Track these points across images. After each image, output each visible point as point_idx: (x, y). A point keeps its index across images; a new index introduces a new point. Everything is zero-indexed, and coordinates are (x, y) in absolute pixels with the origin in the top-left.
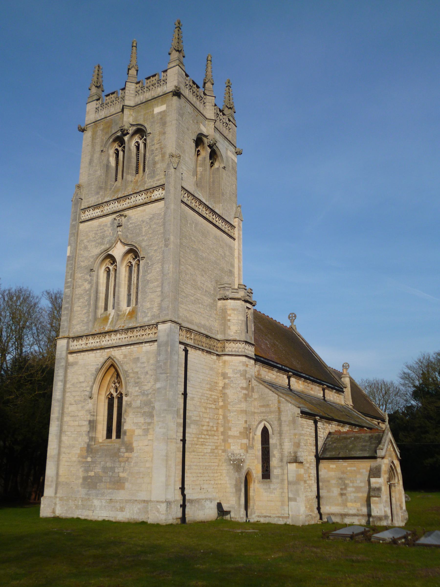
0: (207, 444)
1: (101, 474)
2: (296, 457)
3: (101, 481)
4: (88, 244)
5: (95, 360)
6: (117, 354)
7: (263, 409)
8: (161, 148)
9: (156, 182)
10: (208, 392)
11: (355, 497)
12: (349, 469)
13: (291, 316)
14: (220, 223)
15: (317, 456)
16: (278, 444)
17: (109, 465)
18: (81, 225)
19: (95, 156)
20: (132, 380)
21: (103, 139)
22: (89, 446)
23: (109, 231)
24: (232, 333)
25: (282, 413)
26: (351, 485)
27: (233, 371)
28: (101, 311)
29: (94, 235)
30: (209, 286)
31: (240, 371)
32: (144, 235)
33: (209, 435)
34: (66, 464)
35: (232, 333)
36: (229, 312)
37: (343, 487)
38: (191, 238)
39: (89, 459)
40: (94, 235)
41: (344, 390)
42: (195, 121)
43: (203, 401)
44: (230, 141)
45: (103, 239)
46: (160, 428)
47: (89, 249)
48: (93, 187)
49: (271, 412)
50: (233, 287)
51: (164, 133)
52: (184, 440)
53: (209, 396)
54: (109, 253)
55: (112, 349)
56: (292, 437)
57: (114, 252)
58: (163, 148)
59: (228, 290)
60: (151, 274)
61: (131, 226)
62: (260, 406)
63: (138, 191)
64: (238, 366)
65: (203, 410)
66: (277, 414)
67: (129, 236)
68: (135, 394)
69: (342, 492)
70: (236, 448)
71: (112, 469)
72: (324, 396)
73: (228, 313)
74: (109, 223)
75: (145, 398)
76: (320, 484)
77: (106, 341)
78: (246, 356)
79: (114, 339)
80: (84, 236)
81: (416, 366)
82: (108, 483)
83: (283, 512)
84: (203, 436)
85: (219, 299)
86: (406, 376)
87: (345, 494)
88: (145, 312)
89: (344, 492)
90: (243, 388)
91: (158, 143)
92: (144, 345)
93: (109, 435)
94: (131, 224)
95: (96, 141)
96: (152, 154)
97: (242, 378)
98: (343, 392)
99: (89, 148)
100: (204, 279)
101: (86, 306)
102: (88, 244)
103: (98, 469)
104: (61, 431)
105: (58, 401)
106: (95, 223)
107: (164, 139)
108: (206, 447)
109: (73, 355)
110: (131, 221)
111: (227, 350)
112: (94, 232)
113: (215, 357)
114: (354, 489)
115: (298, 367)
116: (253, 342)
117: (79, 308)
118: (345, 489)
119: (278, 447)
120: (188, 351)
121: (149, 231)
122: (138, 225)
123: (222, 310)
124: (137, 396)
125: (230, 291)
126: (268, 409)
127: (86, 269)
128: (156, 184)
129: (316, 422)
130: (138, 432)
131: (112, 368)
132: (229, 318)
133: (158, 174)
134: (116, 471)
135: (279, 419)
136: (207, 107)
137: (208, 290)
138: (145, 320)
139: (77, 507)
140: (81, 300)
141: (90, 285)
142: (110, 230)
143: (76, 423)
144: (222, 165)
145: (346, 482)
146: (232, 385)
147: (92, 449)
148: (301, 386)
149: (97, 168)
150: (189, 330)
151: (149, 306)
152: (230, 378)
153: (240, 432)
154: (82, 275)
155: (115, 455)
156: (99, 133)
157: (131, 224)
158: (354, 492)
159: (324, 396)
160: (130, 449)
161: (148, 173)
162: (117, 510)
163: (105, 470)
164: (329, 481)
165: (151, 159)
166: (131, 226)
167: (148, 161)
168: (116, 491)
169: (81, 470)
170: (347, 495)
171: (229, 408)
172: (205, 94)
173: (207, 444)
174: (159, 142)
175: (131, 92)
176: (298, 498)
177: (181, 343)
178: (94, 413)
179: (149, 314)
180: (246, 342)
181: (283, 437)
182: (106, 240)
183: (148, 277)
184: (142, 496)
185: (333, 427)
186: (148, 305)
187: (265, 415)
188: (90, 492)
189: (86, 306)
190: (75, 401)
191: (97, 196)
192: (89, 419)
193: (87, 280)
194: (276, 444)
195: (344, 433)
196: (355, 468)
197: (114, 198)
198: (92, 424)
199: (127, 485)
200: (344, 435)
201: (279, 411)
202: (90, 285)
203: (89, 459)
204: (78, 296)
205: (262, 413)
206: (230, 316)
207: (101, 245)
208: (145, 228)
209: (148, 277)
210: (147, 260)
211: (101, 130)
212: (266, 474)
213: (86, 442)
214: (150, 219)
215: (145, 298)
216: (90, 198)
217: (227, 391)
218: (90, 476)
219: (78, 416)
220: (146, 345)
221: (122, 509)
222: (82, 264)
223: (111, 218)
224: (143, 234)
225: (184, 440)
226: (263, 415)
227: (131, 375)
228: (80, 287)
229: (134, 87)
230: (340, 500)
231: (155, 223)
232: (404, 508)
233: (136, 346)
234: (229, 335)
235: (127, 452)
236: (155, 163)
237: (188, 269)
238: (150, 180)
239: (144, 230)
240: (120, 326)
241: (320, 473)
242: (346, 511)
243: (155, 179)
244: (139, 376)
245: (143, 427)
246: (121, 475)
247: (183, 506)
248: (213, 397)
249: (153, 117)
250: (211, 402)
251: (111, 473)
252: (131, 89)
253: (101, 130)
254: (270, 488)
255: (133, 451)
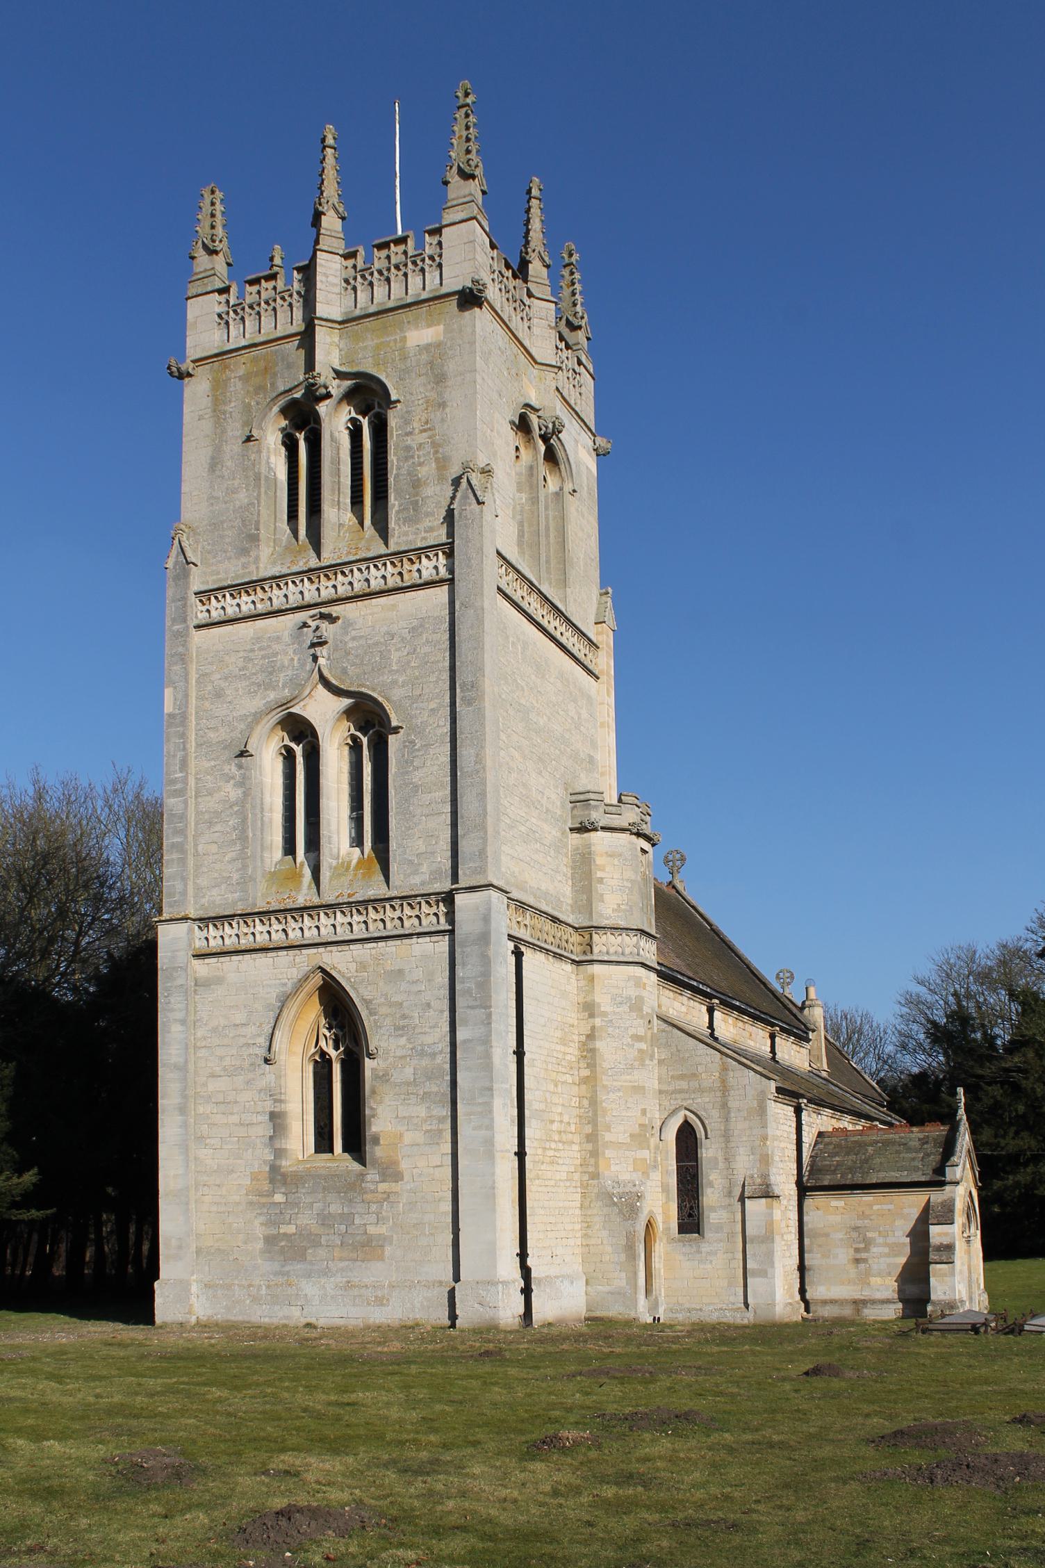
0: (561, 1162)
1: (316, 1229)
2: (768, 1186)
3: (316, 1244)
4: (224, 684)
6: (341, 963)
7: (683, 1085)
8: (435, 445)
9: (423, 535)
10: (559, 1047)
11: (889, 1265)
12: (875, 1207)
13: (670, 857)
14: (569, 639)
15: (799, 1183)
16: (720, 1159)
17: (335, 1208)
18: (198, 637)
19: (226, 448)
20: (388, 1021)
21: (249, 404)
22: (274, 1169)
24: (610, 911)
25: (732, 1092)
26: (881, 1240)
27: (613, 999)
29: (240, 663)
30: (554, 797)
31: (629, 998)
32: (397, 671)
33: (564, 1143)
34: (214, 1208)
35: (610, 911)
36: (599, 861)
37: (862, 1246)
38: (515, 680)
39: (279, 1198)
40: (240, 663)
41: (811, 1035)
42: (513, 372)
43: (550, 1067)
44: (583, 421)
45: (271, 673)
46: (474, 1129)
47: (229, 699)
48: (229, 533)
49: (701, 1090)
50: (607, 801)
51: (442, 405)
53: (560, 1056)
54: (291, 710)
55: (321, 950)
56: (757, 1142)
57: (308, 708)
58: (439, 445)
59: (596, 807)
60: (425, 770)
61: (355, 644)
62: (672, 1077)
63: (370, 555)
64: (632, 989)
65: (551, 1087)
66: (719, 1094)
67: (352, 670)
68: (398, 1054)
69: (858, 1256)
70: (619, 1168)
71: (348, 1219)
72: (773, 1051)
73: (598, 862)
74: (286, 633)
75: (425, 1062)
76: (807, 1241)
77: (308, 928)
78: (644, 965)
80: (211, 664)
81: (935, 978)
82: (337, 1249)
83: (732, 1299)
84: (553, 1145)
85: (571, 830)
86: (913, 1001)
87: (865, 1260)
88: (411, 862)
89: (864, 1255)
90: (637, 1038)
91: (425, 431)
92: (414, 940)
93: (323, 1142)
94: (354, 639)
95: (228, 408)
96: (406, 459)
97: (634, 1014)
98: (808, 1040)
99: (207, 425)
100: (543, 781)
101: (233, 842)
102: (224, 684)
103: (307, 1219)
105: (177, 1067)
107: (443, 420)
108: (559, 1168)
109: (207, 961)
110: (353, 633)
111: (596, 950)
112: (242, 654)
113: (569, 967)
114: (886, 1250)
115: (724, 985)
116: (653, 932)
117: (214, 848)
118: (866, 1249)
119: (721, 1165)
120: (522, 954)
121: (409, 662)
122: (377, 644)
123: (583, 855)
124: (403, 1057)
125: (602, 810)
126: (694, 1084)
127: (225, 748)
128: (424, 538)
129: (798, 1111)
132: (599, 874)
133: (427, 514)
134: (357, 1221)
135: (724, 1106)
136: (535, 330)
137: (550, 807)
138: (413, 882)
139: (256, 1299)
140: (218, 828)
141: (240, 791)
142: (291, 652)
143: (234, 1119)
144: (568, 487)
145: (869, 1235)
146: (610, 1030)
147: (284, 1175)
148: (732, 1029)
149: (236, 482)
150: (522, 906)
151: (423, 849)
152: (605, 1014)
153: (631, 1136)
154: (213, 763)
156: (236, 387)
157: (354, 639)
158: (888, 1255)
159: (773, 1051)
160: (391, 1173)
161: (396, 508)
162: (369, 1304)
163: (325, 1220)
164: (827, 1235)
165: (403, 471)
166: (355, 644)
167: (397, 476)
168: (359, 1263)
169: (257, 1222)
170: (870, 1261)
171: (605, 1083)
172: (530, 295)
173: (561, 1162)
174: (427, 428)
175: (331, 279)
176: (769, 1270)
177: (511, 937)
179: (424, 868)
180: (643, 932)
181: (733, 1145)
182: (282, 678)
183: (417, 777)
186: (421, 846)
187: (687, 1096)
188: (287, 1268)
189: (233, 842)
190: (225, 1069)
191: (243, 560)
192: (268, 1109)
193: (233, 778)
194: (716, 1158)
195: (855, 1132)
196: (891, 1207)
197: (295, 569)
199: (388, 1250)
200: (856, 1138)
201: (725, 1088)
202: (240, 791)
203: (279, 1198)
204: (207, 816)
205: (681, 1091)
206: (603, 870)
207: (266, 689)
208: (398, 654)
209: (417, 777)
210: (408, 735)
211: (240, 378)
212: (691, 1222)
213: (264, 1161)
214: (413, 630)
215: (409, 828)
216: (220, 562)
217: (599, 1044)
218: (285, 1234)
219: (236, 1102)
220: (420, 940)
221: (380, 1302)
222: (212, 735)
224: (395, 668)
226: (683, 1095)
227: (384, 1010)
228: (210, 794)
229: (339, 266)
230: (852, 1271)
231: (427, 641)
232: (982, 1286)
233: (390, 943)
234: (601, 915)
235: (383, 1181)
236: (416, 484)
237: (512, 758)
238: (406, 528)
239: (395, 656)
240: (341, 895)
241: (806, 1218)
242: (866, 1294)
243: (421, 526)
244: (406, 1012)
245: (426, 1127)
246: (372, 1230)
247: (527, 1291)
248: (568, 1057)
249: (404, 358)
250: (564, 1070)
251: (343, 1227)
252: (332, 272)
253: (240, 378)
254: (699, 1252)
255: (402, 1179)
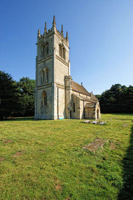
5: (42, 91)
6: (45, 89)
23: (43, 66)
28: (42, 82)
52: (58, 105)
77: (43, 87)
79: (45, 87)
93: (45, 105)
104: (37, 104)
106: (40, 64)
129: (84, 101)
130: (49, 104)
131: (44, 92)
150: (58, 84)
155: (46, 108)
163: (44, 110)
178: (42, 100)
184: (50, 115)
185: (87, 102)
198: (42, 103)
212: (74, 111)
221: (47, 117)
223: (43, 63)
225: (58, 105)
247: (58, 117)
